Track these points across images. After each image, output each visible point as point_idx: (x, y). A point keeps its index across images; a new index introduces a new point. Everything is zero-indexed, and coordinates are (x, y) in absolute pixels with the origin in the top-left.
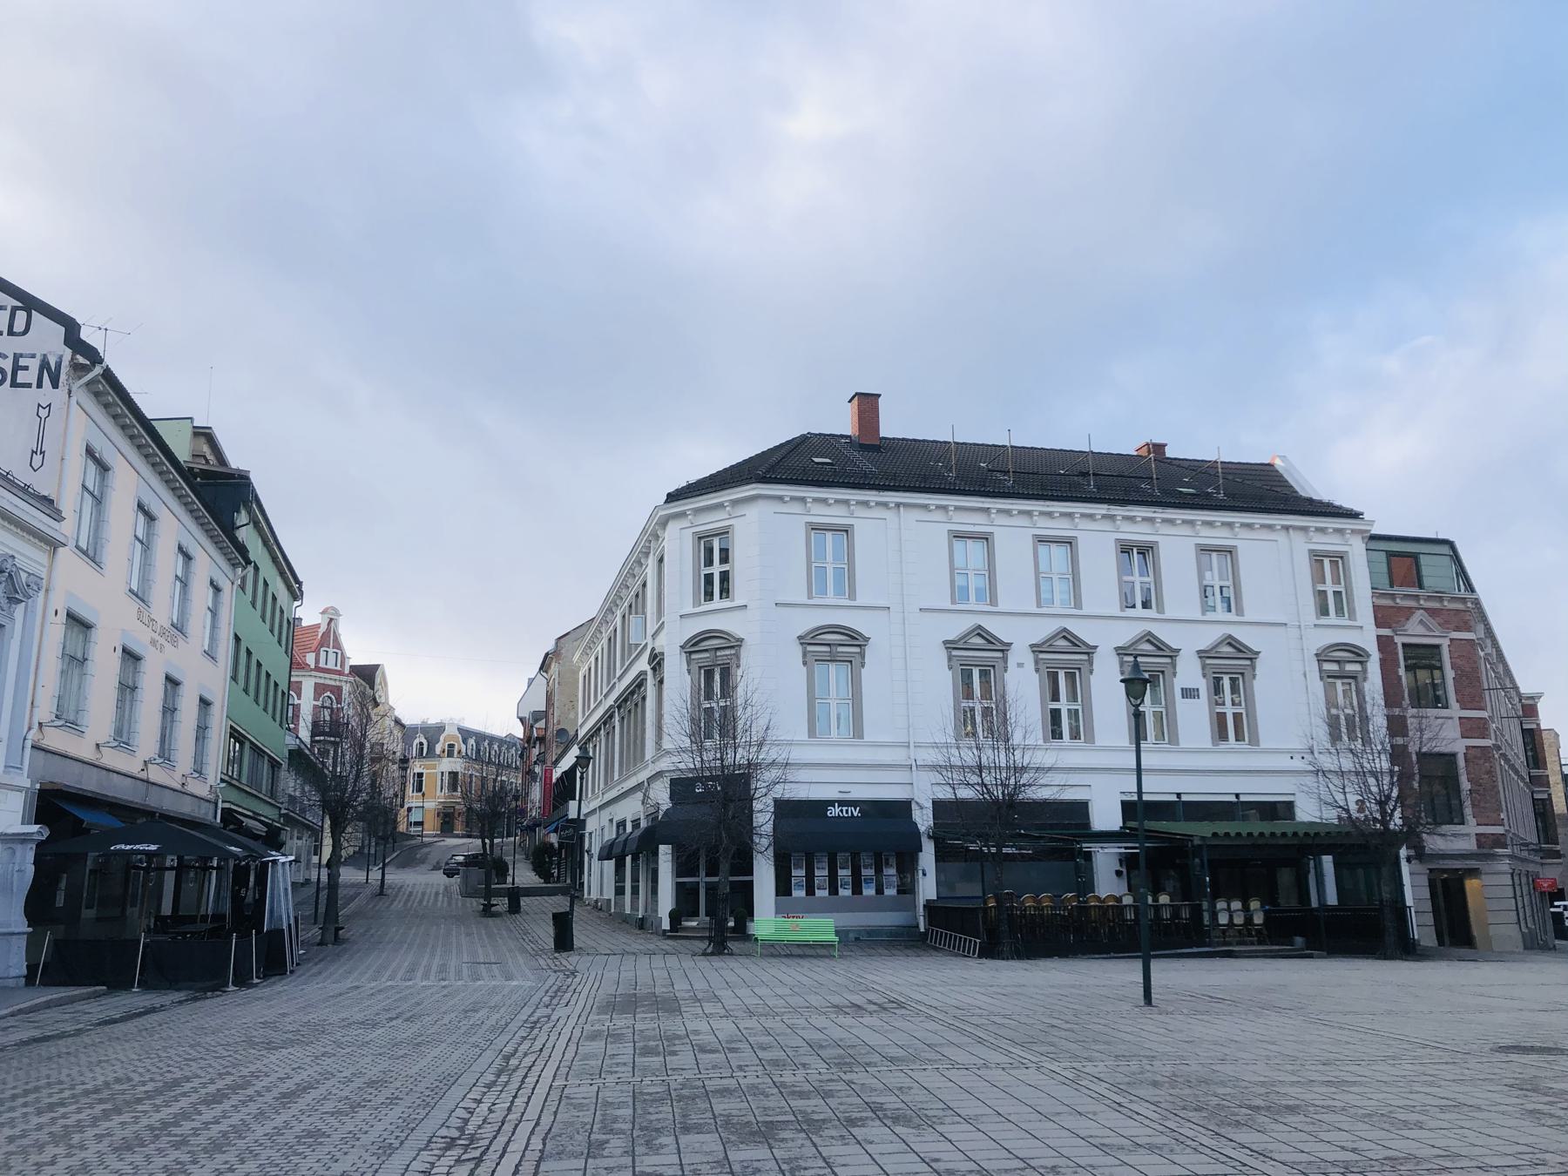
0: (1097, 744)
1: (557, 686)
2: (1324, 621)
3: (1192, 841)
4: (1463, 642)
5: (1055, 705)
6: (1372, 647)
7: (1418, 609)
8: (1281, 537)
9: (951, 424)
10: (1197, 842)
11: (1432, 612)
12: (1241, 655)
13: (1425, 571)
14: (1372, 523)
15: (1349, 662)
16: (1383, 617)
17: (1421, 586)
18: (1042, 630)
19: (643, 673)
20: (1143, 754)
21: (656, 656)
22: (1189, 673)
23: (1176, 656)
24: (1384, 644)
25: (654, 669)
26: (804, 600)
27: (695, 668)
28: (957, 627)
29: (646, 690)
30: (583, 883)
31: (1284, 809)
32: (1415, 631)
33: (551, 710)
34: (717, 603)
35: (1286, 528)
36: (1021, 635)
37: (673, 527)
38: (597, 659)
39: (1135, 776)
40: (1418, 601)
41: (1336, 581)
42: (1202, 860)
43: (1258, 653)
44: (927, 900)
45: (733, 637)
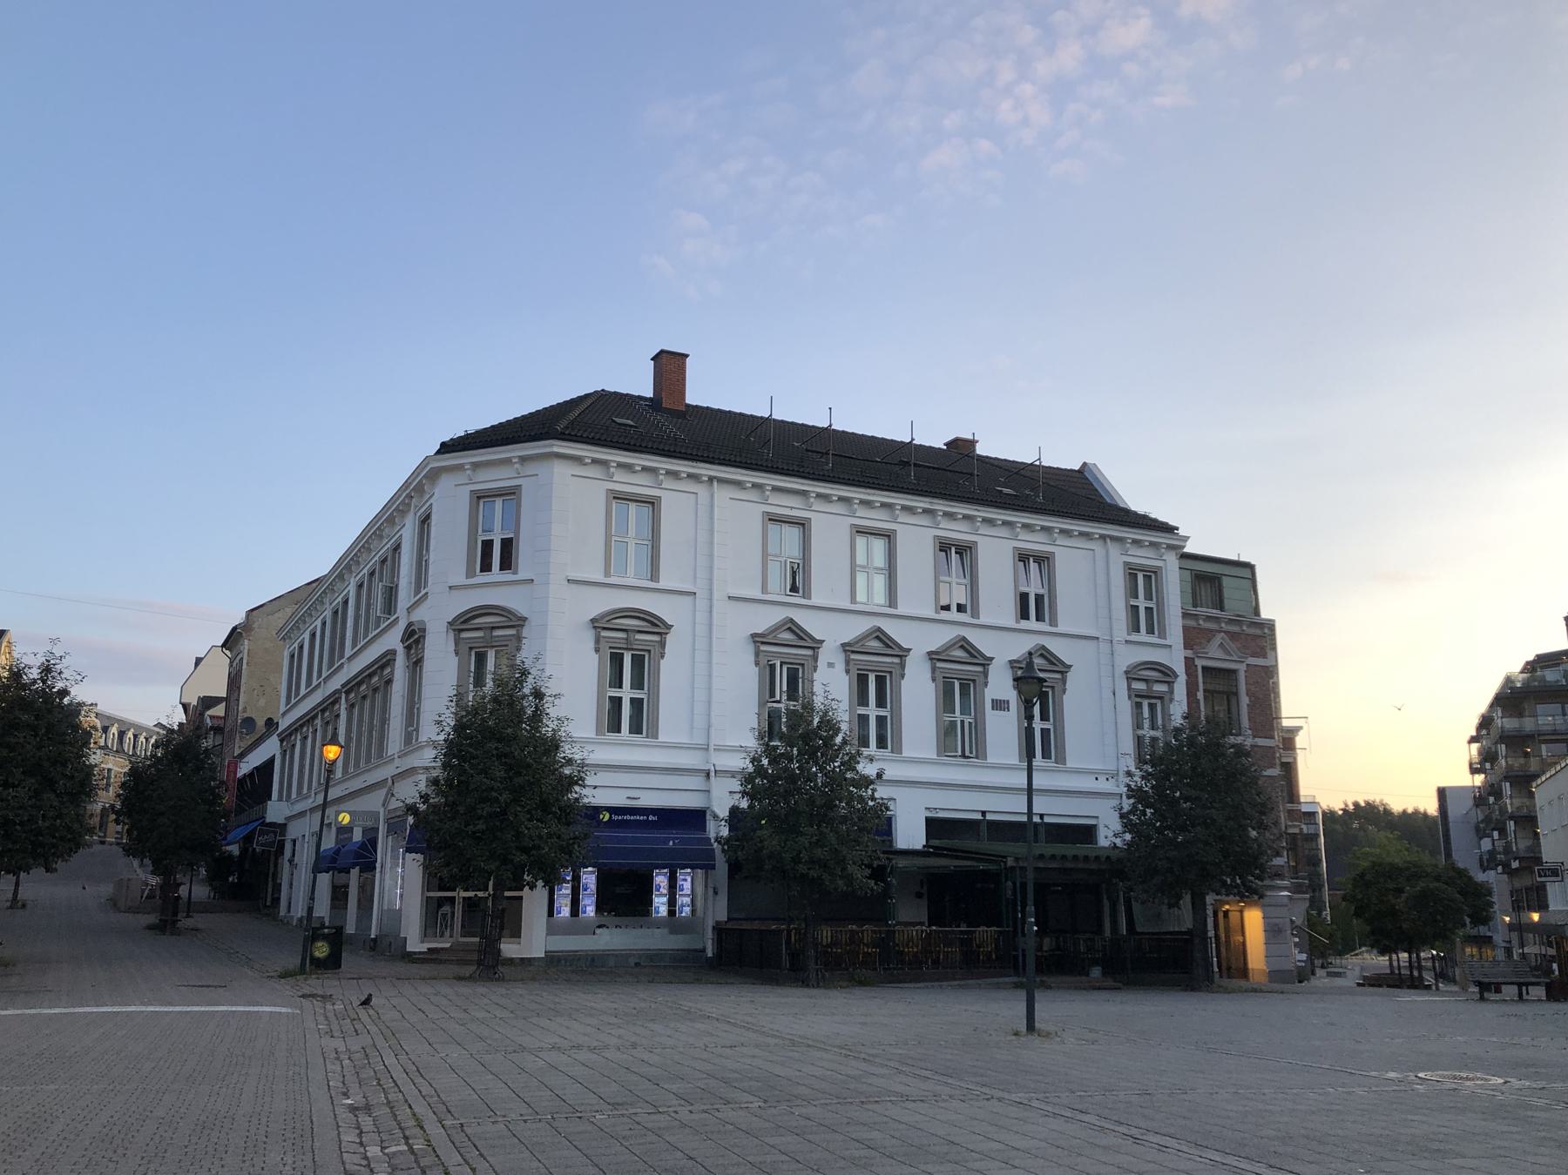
0: (1068, 765)
1: (244, 666)
2: (1135, 637)
3: (1005, 863)
4: (1257, 668)
5: (862, 711)
6: (1180, 668)
7: (1220, 632)
8: (1096, 546)
9: (827, 408)
10: (1010, 862)
11: (1233, 636)
12: (889, 651)
13: (1226, 593)
14: (1186, 539)
15: (1157, 681)
16: (1193, 638)
17: (1222, 609)
18: (854, 629)
19: (393, 652)
20: (1034, 774)
21: (413, 633)
22: (1000, 685)
23: (988, 665)
24: (1189, 663)
25: (408, 648)
26: (600, 578)
27: (464, 648)
28: (766, 619)
29: (392, 673)
30: (279, 899)
31: (1086, 833)
32: (1215, 654)
33: (236, 694)
34: (496, 574)
35: (1103, 537)
36: (920, 640)
37: (445, 484)
38: (313, 635)
39: (1026, 797)
40: (1197, 620)
41: (1148, 597)
42: (1014, 884)
43: (1071, 666)
44: (717, 921)
45: (515, 615)
